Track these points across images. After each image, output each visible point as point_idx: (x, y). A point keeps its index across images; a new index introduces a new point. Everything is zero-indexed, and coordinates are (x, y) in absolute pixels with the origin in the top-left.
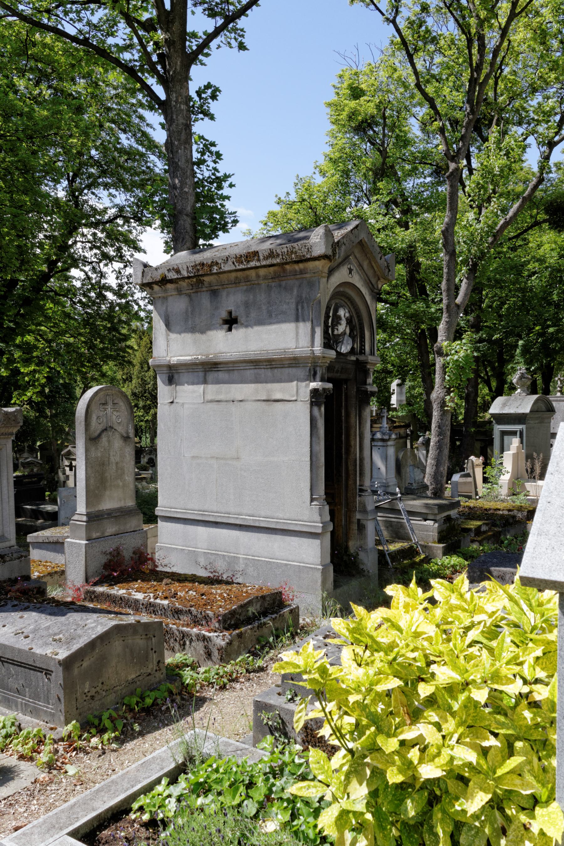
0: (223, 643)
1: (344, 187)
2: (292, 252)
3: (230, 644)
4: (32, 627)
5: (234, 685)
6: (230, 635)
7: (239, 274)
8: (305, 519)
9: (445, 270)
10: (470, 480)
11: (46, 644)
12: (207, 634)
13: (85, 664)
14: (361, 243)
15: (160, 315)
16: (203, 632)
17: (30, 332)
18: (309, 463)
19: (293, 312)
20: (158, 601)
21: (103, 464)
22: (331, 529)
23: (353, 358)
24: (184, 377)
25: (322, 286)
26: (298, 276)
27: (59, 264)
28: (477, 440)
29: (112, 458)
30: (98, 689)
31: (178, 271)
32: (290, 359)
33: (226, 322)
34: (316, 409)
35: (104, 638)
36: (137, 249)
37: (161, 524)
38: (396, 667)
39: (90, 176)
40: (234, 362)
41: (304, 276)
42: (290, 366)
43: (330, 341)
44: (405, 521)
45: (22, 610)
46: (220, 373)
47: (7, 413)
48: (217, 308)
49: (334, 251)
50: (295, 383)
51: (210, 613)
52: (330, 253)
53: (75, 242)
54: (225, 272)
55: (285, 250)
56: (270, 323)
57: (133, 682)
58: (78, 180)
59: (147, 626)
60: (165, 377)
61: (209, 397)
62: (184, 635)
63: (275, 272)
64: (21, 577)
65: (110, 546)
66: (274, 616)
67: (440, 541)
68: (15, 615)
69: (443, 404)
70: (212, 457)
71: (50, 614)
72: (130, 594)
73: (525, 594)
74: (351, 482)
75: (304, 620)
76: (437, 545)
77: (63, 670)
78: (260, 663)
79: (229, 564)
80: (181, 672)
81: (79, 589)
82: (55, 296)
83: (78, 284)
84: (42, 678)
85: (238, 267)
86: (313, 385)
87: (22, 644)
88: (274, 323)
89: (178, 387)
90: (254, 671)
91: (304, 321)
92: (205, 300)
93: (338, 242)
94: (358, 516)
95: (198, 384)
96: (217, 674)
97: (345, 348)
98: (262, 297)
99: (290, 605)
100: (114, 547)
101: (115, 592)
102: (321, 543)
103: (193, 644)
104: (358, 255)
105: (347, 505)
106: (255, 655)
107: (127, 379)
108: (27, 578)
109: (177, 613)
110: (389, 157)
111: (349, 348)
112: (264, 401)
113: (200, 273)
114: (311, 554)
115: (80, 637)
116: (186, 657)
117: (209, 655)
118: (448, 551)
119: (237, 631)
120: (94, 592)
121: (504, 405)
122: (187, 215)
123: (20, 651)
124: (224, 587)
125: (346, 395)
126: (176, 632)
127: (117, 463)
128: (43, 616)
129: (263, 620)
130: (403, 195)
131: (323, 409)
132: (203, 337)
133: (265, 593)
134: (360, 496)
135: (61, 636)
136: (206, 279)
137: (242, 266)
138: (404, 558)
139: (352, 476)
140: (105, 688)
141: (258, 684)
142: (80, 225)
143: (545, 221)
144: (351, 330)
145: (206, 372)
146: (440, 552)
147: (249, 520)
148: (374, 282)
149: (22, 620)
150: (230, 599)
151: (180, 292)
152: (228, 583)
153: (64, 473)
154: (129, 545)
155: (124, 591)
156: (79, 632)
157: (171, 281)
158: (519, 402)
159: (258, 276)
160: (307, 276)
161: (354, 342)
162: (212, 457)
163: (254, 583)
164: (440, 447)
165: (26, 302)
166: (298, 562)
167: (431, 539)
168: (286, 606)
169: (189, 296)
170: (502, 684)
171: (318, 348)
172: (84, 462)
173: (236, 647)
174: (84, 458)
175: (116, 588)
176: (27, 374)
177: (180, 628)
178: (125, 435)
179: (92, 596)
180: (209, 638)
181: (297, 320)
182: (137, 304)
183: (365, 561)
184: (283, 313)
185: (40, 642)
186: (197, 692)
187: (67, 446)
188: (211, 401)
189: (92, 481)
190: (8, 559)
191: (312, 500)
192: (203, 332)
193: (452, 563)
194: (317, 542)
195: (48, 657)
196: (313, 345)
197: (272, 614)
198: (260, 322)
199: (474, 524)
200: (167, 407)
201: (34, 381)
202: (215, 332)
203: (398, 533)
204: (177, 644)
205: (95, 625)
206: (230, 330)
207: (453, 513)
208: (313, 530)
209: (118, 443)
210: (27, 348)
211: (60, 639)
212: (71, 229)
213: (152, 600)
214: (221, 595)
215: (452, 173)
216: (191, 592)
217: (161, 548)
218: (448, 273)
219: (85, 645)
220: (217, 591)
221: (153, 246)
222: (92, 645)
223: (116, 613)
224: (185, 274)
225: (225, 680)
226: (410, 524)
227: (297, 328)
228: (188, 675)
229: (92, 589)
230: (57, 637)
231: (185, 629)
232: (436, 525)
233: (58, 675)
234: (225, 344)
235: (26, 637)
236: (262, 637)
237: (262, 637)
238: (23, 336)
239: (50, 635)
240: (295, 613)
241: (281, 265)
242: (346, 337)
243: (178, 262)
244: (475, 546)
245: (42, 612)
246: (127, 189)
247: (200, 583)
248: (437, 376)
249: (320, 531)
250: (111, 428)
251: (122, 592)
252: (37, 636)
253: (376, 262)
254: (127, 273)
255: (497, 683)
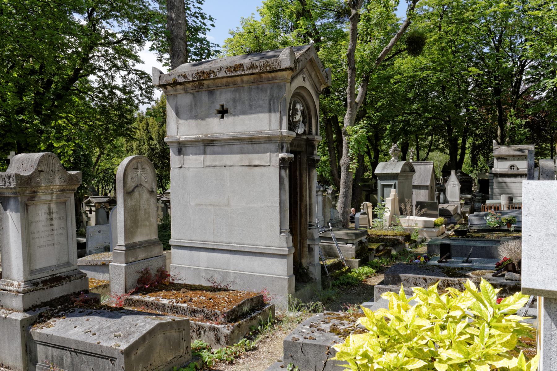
0: (228, 332)
1: (275, 25)
2: (267, 65)
3: (233, 332)
4: (97, 327)
5: (238, 360)
6: (233, 326)
7: (229, 79)
8: (276, 245)
9: (349, 80)
10: (366, 216)
11: (110, 339)
12: (216, 326)
13: (139, 352)
14: (311, 60)
15: (171, 106)
16: (214, 325)
17: (61, 118)
18: (279, 208)
19: (267, 106)
20: (179, 304)
21: (136, 210)
22: (294, 252)
23: (305, 137)
24: (190, 149)
25: (287, 89)
26: (271, 82)
27: (81, 72)
28: (364, 190)
29: (142, 206)
30: (148, 369)
31: (185, 77)
32: (265, 138)
33: (219, 112)
34: (283, 172)
35: (151, 333)
36: (138, 61)
37: (173, 250)
38: (415, 351)
39: (104, 10)
40: (225, 140)
41: (275, 81)
42: (265, 142)
43: (292, 126)
44: (335, 245)
45: (86, 315)
46: (215, 147)
47: (70, 175)
48: (213, 103)
49: (295, 65)
50: (269, 154)
51: (218, 312)
52: (293, 66)
53: (94, 56)
54: (219, 78)
55: (262, 64)
56: (251, 114)
57: (171, 362)
58: (95, 14)
59: (179, 322)
60: (176, 150)
61: (208, 163)
62: (200, 327)
63: (254, 78)
64: (83, 291)
65: (141, 267)
66: (259, 312)
67: (356, 258)
68: (83, 319)
69: (348, 168)
70: (210, 205)
71: (109, 317)
72: (159, 300)
73: (487, 295)
74: (303, 220)
75: (277, 313)
76: (355, 260)
77: (125, 357)
78: (253, 344)
79: (223, 277)
80: (201, 353)
81: (120, 298)
82: (80, 93)
83: (96, 85)
84: (108, 363)
85: (229, 75)
86: (281, 155)
87: (92, 340)
88: (254, 113)
89: (185, 157)
90: (250, 350)
91: (275, 112)
92: (204, 97)
93: (298, 59)
94: (308, 242)
95: (199, 154)
96: (226, 353)
97: (300, 131)
98: (245, 96)
99: (268, 304)
100: (144, 267)
101: (148, 299)
102: (288, 261)
103: (206, 333)
104: (308, 68)
105: (301, 235)
106: (250, 338)
107: (130, 150)
108: (87, 292)
109: (194, 312)
110: (306, 5)
111: (303, 130)
112: (247, 166)
113: (202, 78)
114: (280, 269)
115: (134, 333)
116: (201, 342)
117: (218, 340)
118: (362, 264)
119: (237, 323)
120: (132, 300)
121: (384, 168)
122: (181, 39)
123: (90, 344)
124: (224, 293)
125: (300, 161)
126: (193, 325)
127: (145, 209)
128: (104, 318)
129: (253, 315)
130: (315, 29)
131: (288, 171)
132: (203, 122)
133: (253, 296)
134: (310, 229)
135: (120, 333)
136: (205, 82)
137: (231, 74)
138: (336, 269)
139: (304, 216)
140: (153, 368)
141: (254, 359)
142: (97, 45)
143: (405, 50)
144: (304, 119)
145: (205, 146)
146: (357, 265)
147: (237, 247)
148: (318, 86)
149: (88, 322)
150: (230, 301)
151: (186, 91)
152: (226, 290)
153: (87, 216)
154: (154, 266)
155: (154, 298)
156: (133, 329)
157: (180, 84)
158: (393, 166)
159: (242, 81)
160: (277, 81)
161: (305, 126)
162: (210, 205)
163: (244, 290)
164: (346, 195)
165: (59, 97)
166: (272, 275)
167: (351, 256)
168: (266, 305)
169: (193, 94)
170: (494, 361)
171: (285, 130)
172: (123, 209)
173: (236, 334)
174: (123, 206)
175: (148, 296)
176: (59, 148)
177: (197, 323)
178: (150, 190)
179: (130, 302)
180: (218, 329)
181: (270, 111)
182: (137, 99)
183: (313, 271)
184: (261, 106)
185: (105, 338)
186: (213, 367)
187: (88, 197)
188: (209, 166)
189: (129, 222)
190: (73, 279)
191: (281, 232)
192: (203, 119)
193: (365, 271)
194: (285, 261)
195: (113, 349)
196: (281, 128)
197: (257, 310)
198: (244, 113)
199: (374, 246)
200: (177, 170)
201: (64, 153)
202: (212, 119)
203: (330, 253)
204: (195, 334)
205: (144, 324)
206: (222, 117)
207: (363, 238)
208: (282, 253)
209: (146, 195)
210: (59, 129)
211: (120, 335)
212: (90, 47)
213: (175, 304)
214: (223, 299)
215: (353, 17)
216: (201, 298)
217: (175, 268)
218: (350, 82)
219: (139, 339)
220: (220, 296)
221: (150, 59)
222: (143, 338)
223: (157, 315)
224: (191, 79)
225: (232, 358)
226: (338, 247)
227: (270, 117)
228: (205, 354)
229: (130, 297)
230: (117, 334)
231: (200, 323)
232: (354, 247)
233: (121, 361)
234: (217, 127)
235: (94, 334)
236: (252, 326)
237: (252, 326)
238: (56, 121)
239: (112, 333)
240: (272, 308)
241: (259, 74)
242: (301, 123)
243: (184, 70)
244: (376, 260)
245: (102, 316)
246: (130, 19)
247: (207, 291)
248: (343, 149)
249: (286, 253)
250: (141, 185)
251: (152, 299)
252: (102, 333)
253: (320, 73)
254: (130, 78)
255: (490, 360)
